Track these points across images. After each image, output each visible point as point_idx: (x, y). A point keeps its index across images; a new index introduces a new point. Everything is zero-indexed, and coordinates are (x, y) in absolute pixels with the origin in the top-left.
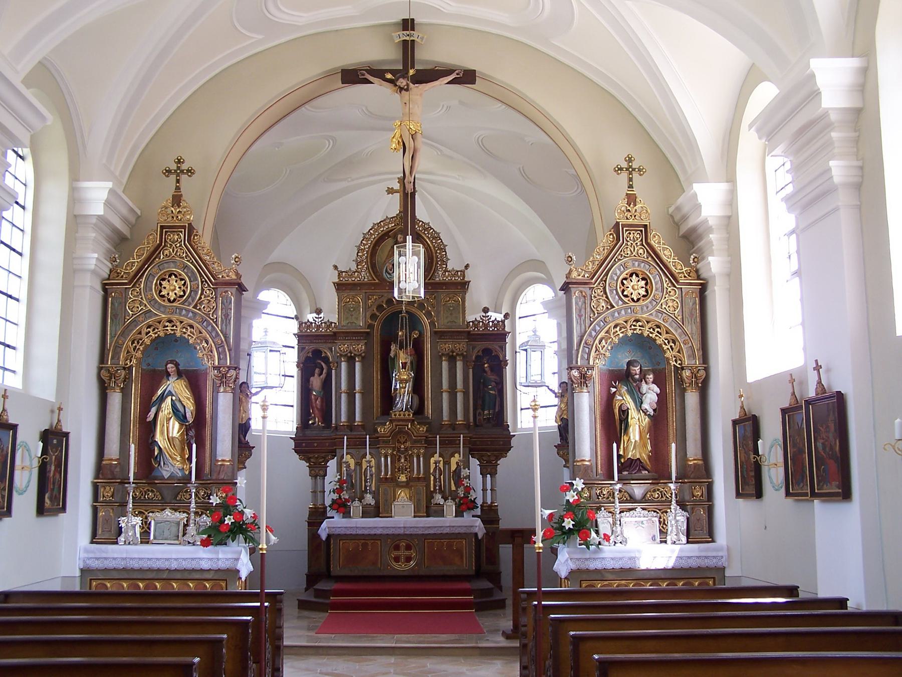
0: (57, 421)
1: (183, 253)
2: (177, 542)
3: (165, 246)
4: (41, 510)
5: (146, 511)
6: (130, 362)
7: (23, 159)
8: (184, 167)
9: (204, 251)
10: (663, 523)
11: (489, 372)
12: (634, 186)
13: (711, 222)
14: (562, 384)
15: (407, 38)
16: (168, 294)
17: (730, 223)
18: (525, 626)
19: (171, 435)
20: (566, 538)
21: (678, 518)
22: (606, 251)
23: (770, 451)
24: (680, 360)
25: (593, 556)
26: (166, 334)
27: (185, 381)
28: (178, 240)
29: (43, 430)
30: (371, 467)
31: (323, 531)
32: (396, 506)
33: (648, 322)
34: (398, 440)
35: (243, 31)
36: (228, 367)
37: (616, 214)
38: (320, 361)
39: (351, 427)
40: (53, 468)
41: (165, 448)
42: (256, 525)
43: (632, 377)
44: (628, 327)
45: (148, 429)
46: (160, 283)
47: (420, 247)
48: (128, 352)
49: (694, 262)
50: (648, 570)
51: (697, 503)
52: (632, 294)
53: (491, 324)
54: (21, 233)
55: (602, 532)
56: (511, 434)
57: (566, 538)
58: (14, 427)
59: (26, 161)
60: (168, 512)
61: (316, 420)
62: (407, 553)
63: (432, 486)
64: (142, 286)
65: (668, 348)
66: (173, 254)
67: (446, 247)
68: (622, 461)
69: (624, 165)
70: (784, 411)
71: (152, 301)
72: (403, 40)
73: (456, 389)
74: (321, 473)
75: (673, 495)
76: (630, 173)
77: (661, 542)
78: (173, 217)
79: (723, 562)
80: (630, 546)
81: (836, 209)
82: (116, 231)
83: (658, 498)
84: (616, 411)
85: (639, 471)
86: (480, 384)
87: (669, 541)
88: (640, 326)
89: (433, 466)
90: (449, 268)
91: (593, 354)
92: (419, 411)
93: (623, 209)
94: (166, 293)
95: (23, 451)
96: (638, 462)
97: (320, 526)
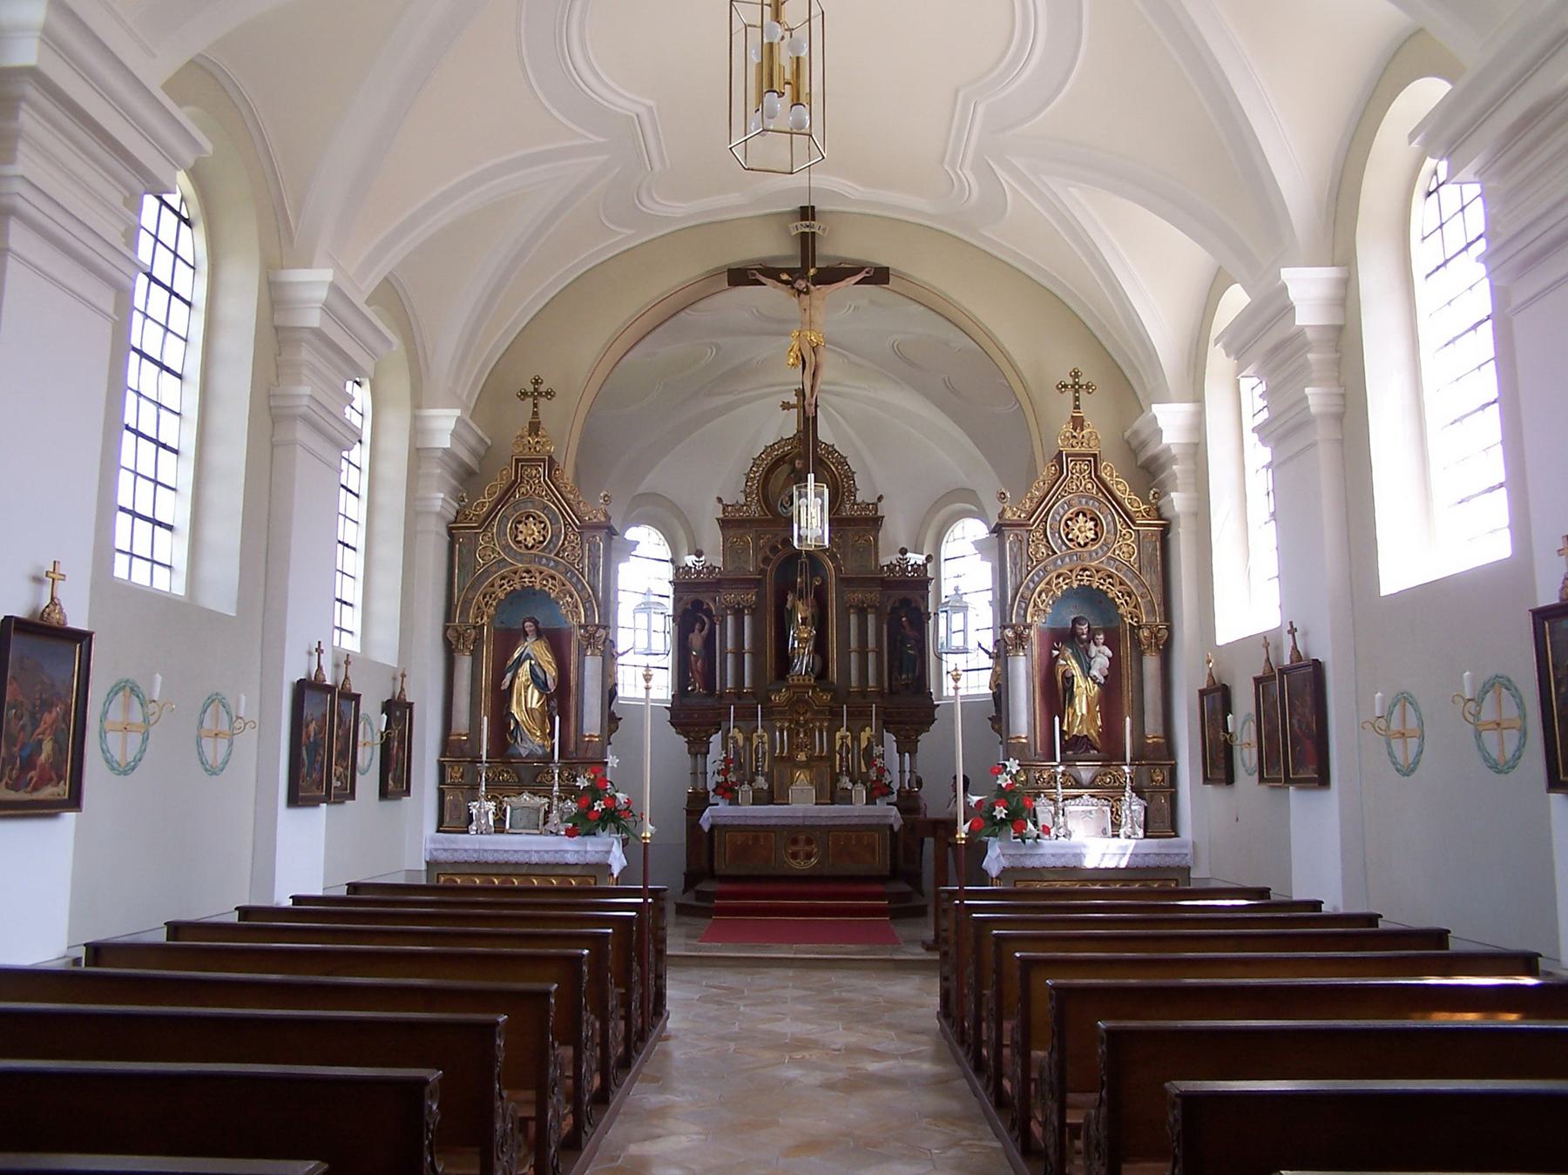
0: (400, 689)
1: (543, 491)
2: (536, 832)
3: (521, 482)
4: (384, 794)
5: (501, 795)
6: (482, 620)
7: (360, 386)
8: (543, 388)
9: (566, 488)
10: (1116, 814)
11: (908, 629)
12: (1081, 407)
13: (1174, 451)
14: (996, 643)
15: (807, 230)
16: (525, 540)
17: (1197, 451)
18: (945, 930)
19: (529, 706)
20: (997, 830)
21: (1133, 808)
22: (1046, 485)
23: (1243, 728)
24: (1137, 617)
25: (1030, 852)
26: (523, 587)
27: (545, 642)
28: (536, 476)
29: (385, 700)
30: (763, 743)
31: (705, 823)
32: (794, 791)
33: (1098, 572)
34: (796, 711)
35: (612, 227)
36: (596, 625)
37: (1059, 441)
38: (700, 614)
39: (738, 693)
40: (396, 744)
41: (523, 721)
42: (631, 811)
43: (1079, 637)
44: (1074, 578)
45: (502, 698)
46: (516, 526)
47: (823, 487)
48: (479, 608)
49: (1154, 498)
50: (1096, 869)
51: (1157, 790)
52: (1078, 537)
53: (910, 568)
54: (358, 471)
55: (1041, 823)
56: (936, 703)
57: (997, 830)
58: (357, 697)
59: (363, 387)
60: (525, 796)
61: (696, 687)
62: (808, 848)
63: (838, 766)
64: (495, 530)
65: (1122, 603)
66: (531, 492)
67: (855, 475)
68: (1067, 738)
69: (1070, 381)
70: (1258, 681)
71: (506, 547)
72: (803, 233)
73: (867, 647)
74: (704, 750)
75: (1128, 780)
76: (1077, 391)
77: (1113, 836)
78: (530, 449)
79: (1188, 861)
80: (1075, 839)
81: (1313, 445)
82: (462, 464)
83: (1110, 782)
84: (1060, 678)
85: (1087, 750)
86: (896, 643)
87: (1122, 836)
88: (1087, 576)
89: (838, 743)
90: (859, 500)
91: (1030, 610)
92: (822, 674)
93: (1067, 435)
94: (523, 538)
95: (364, 724)
96: (1085, 739)
97: (702, 815)
